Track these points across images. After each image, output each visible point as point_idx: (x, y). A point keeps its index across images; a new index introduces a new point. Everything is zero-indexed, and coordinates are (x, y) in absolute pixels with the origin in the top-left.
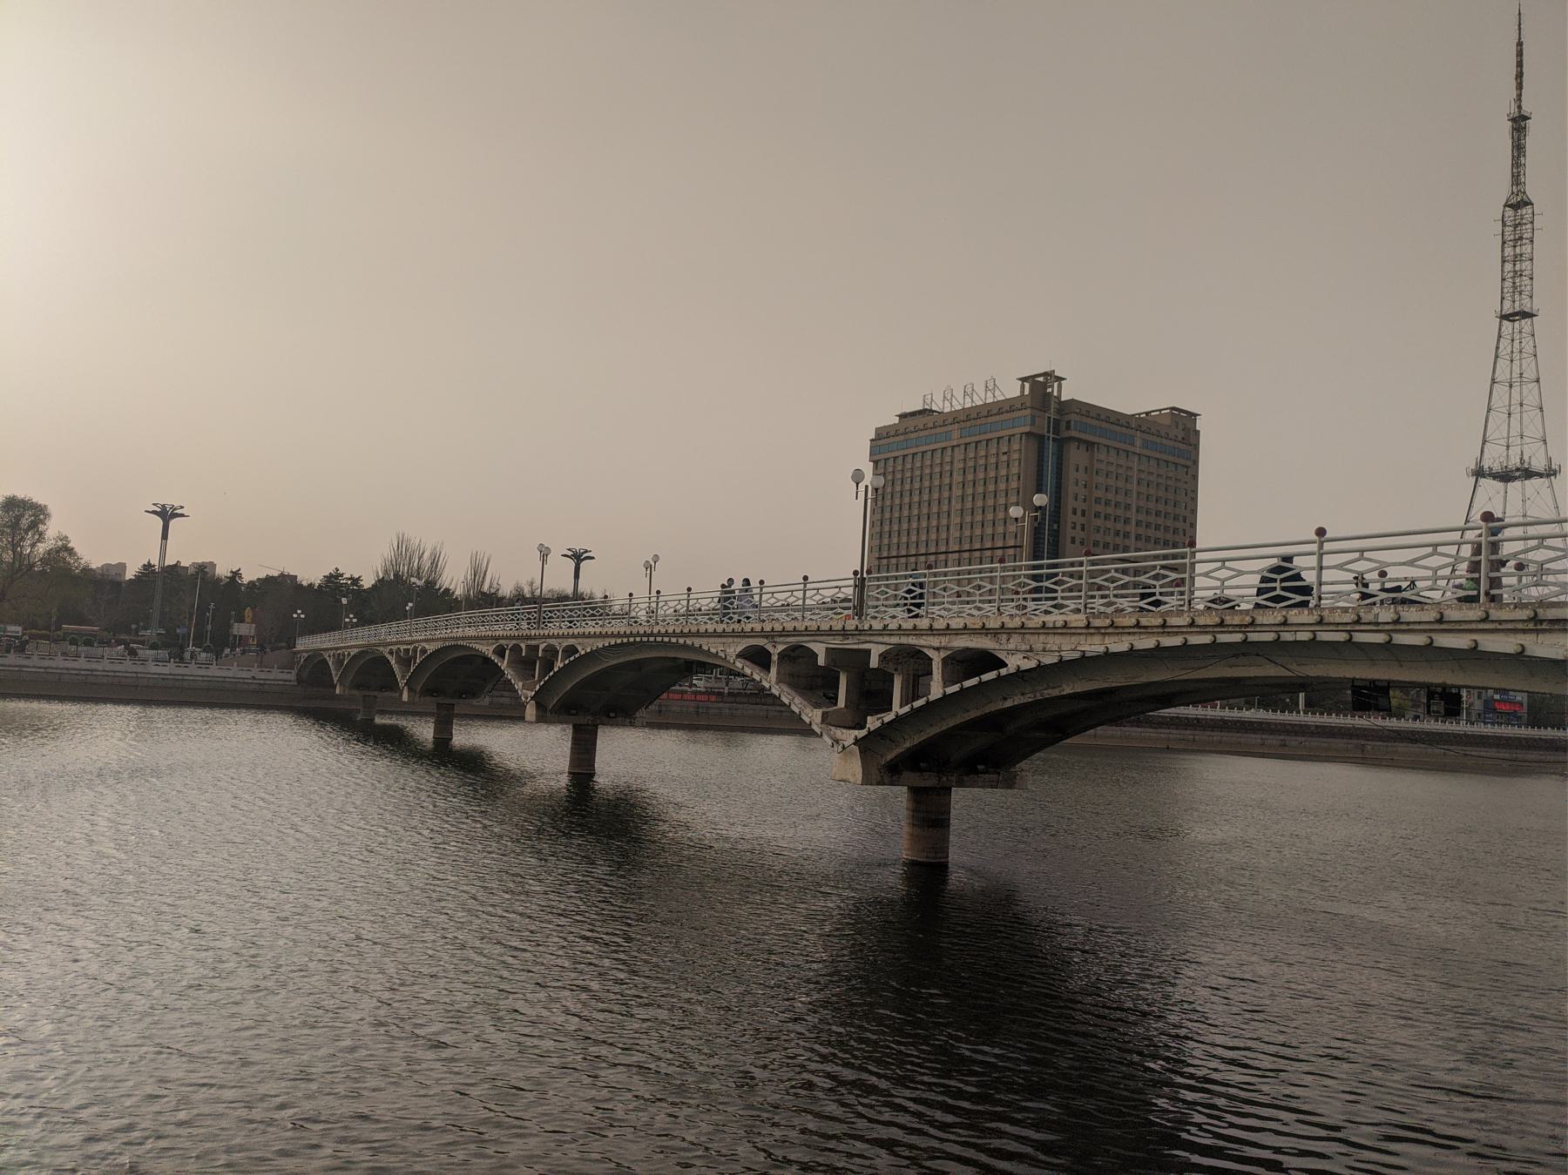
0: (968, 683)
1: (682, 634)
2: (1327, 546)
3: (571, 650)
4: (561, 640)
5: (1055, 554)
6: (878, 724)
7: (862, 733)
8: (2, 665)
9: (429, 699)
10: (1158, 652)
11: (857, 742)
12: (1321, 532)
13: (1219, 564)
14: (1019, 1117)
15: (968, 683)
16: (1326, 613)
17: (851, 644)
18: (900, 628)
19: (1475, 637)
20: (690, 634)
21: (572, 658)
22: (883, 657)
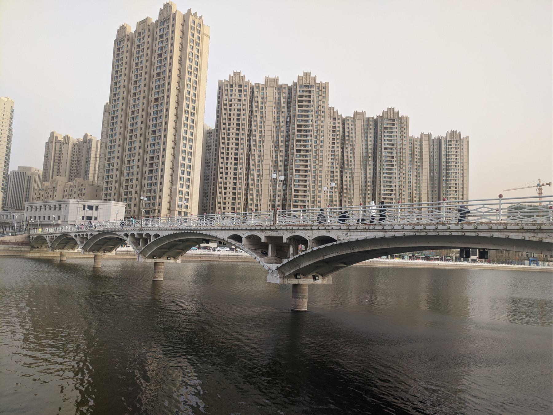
0: (321, 247)
1: (207, 230)
2: (502, 201)
3: (157, 236)
4: (244, 232)
5: (28, 201)
6: (287, 262)
7: (279, 265)
8: (552, 232)
9: (91, 253)
10: (385, 239)
11: (278, 269)
12: (500, 196)
13: (482, 206)
14: (369, 399)
15: (321, 247)
16: (277, 227)
17: (274, 234)
18: (276, 229)
19: (493, 233)
20: (211, 230)
21: (157, 238)
22: (289, 239)
